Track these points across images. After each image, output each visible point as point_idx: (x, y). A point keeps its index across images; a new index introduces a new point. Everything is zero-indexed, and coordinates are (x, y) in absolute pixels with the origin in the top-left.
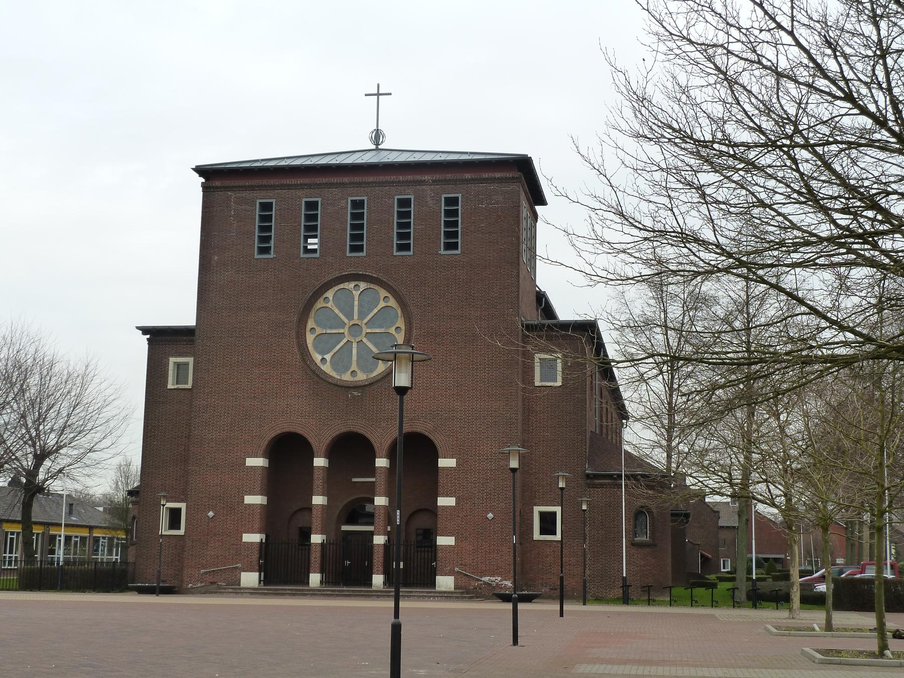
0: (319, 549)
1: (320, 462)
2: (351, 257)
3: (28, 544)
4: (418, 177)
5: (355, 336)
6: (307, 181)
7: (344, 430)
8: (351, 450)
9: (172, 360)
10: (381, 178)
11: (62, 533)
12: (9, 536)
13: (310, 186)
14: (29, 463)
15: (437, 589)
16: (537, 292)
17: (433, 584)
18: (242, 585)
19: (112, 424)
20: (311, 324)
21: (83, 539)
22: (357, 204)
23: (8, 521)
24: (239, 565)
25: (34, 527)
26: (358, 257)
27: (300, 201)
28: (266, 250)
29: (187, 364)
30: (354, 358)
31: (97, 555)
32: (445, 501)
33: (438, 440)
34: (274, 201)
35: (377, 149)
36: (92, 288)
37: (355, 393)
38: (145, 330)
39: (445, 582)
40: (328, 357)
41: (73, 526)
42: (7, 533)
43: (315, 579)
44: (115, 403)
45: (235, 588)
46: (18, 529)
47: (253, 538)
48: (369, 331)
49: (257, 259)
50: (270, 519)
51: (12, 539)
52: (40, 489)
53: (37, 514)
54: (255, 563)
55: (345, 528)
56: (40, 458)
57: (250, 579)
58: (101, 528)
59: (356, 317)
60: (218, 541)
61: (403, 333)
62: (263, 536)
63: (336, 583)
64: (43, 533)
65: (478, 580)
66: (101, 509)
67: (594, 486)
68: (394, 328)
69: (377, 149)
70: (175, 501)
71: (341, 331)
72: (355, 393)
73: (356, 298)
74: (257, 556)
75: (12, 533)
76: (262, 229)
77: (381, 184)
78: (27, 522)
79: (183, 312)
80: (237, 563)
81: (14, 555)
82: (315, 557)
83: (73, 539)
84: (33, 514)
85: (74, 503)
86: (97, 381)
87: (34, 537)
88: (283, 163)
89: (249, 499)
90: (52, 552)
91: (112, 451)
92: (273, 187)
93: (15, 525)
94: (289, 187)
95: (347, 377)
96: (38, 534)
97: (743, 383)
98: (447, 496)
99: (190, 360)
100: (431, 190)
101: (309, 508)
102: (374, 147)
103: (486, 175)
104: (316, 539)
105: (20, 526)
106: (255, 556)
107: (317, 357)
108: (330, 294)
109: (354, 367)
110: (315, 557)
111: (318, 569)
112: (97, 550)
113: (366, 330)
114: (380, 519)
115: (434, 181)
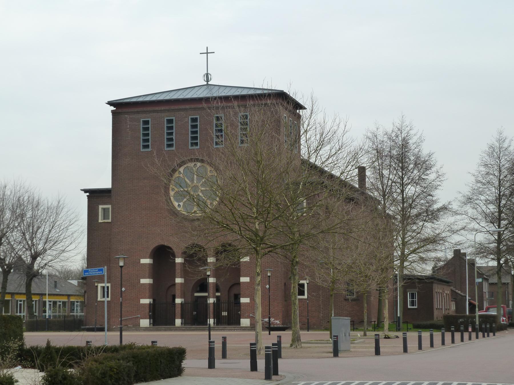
0: (180, 306)
1: (179, 260)
2: (191, 149)
3: (30, 307)
9: (101, 207)
11: (47, 300)
12: (19, 303)
13: (168, 111)
14: (29, 260)
15: (241, 325)
16: (302, 160)
17: (239, 323)
19: (75, 235)
21: (64, 303)
22: (194, 120)
23: (17, 294)
24: (139, 316)
25: (33, 296)
27: (164, 119)
28: (147, 147)
29: (109, 209)
31: (74, 313)
34: (150, 119)
38: (86, 191)
40: (181, 204)
41: (54, 295)
42: (17, 301)
43: (211, 321)
44: (76, 223)
46: (24, 298)
47: (146, 301)
49: (142, 152)
50: (155, 291)
51: (20, 304)
52: (36, 274)
53: (34, 289)
55: (196, 294)
56: (34, 258)
57: (145, 323)
58: (75, 295)
62: (151, 300)
64: (39, 300)
66: (75, 282)
69: (207, 84)
75: (21, 301)
78: (29, 294)
79: (105, 182)
80: (138, 315)
81: (22, 314)
82: (178, 310)
83: (58, 303)
84: (32, 289)
85: (56, 280)
86: (65, 210)
87: (34, 303)
89: (143, 281)
90: (45, 311)
91: (75, 252)
92: (150, 112)
93: (22, 296)
94: (157, 111)
96: (36, 301)
98: (245, 276)
99: (109, 206)
101: (174, 284)
102: (206, 83)
104: (178, 301)
105: (25, 296)
106: (147, 310)
107: (176, 204)
110: (178, 310)
111: (180, 317)
112: (74, 310)
114: (211, 289)
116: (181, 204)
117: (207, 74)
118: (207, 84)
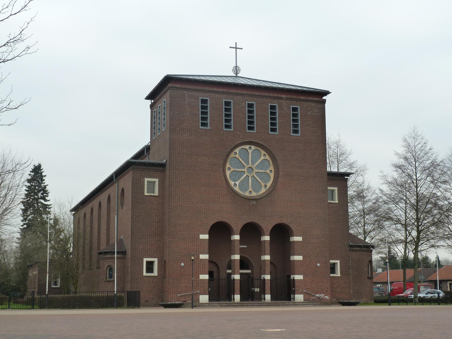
2: (249, 133)
4: (279, 95)
5: (250, 173)
6: (225, 90)
7: (249, 221)
8: (251, 231)
9: (146, 180)
10: (183, 86)
13: (226, 93)
18: (296, 301)
20: (228, 165)
22: (251, 106)
24: (198, 292)
26: (252, 133)
30: (250, 184)
32: (298, 258)
33: (293, 227)
35: (236, 76)
36: (87, 136)
37: (254, 203)
39: (299, 298)
40: (237, 183)
43: (237, 298)
45: (195, 304)
48: (257, 171)
49: (201, 129)
54: (207, 290)
55: (249, 271)
57: (204, 298)
59: (250, 163)
60: (187, 279)
61: (273, 173)
63: (247, 299)
65: (314, 296)
67: (353, 251)
68: (269, 170)
70: (151, 257)
71: (243, 170)
72: (254, 203)
73: (250, 154)
74: (207, 286)
76: (294, 121)
77: (262, 96)
88: (198, 78)
92: (209, 92)
95: (247, 194)
97: (33, 189)
98: (299, 255)
99: (157, 180)
100: (286, 103)
103: (310, 99)
107: (232, 183)
108: (237, 150)
109: (250, 189)
110: (237, 286)
111: (239, 293)
113: (255, 170)
115: (287, 98)
116: (237, 183)
117: (236, 67)
118: (236, 76)
